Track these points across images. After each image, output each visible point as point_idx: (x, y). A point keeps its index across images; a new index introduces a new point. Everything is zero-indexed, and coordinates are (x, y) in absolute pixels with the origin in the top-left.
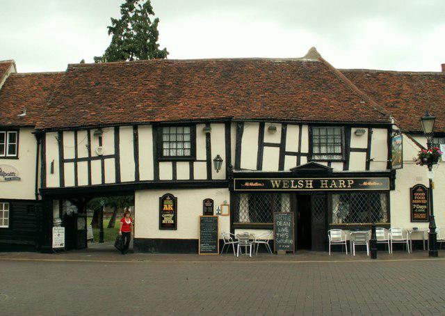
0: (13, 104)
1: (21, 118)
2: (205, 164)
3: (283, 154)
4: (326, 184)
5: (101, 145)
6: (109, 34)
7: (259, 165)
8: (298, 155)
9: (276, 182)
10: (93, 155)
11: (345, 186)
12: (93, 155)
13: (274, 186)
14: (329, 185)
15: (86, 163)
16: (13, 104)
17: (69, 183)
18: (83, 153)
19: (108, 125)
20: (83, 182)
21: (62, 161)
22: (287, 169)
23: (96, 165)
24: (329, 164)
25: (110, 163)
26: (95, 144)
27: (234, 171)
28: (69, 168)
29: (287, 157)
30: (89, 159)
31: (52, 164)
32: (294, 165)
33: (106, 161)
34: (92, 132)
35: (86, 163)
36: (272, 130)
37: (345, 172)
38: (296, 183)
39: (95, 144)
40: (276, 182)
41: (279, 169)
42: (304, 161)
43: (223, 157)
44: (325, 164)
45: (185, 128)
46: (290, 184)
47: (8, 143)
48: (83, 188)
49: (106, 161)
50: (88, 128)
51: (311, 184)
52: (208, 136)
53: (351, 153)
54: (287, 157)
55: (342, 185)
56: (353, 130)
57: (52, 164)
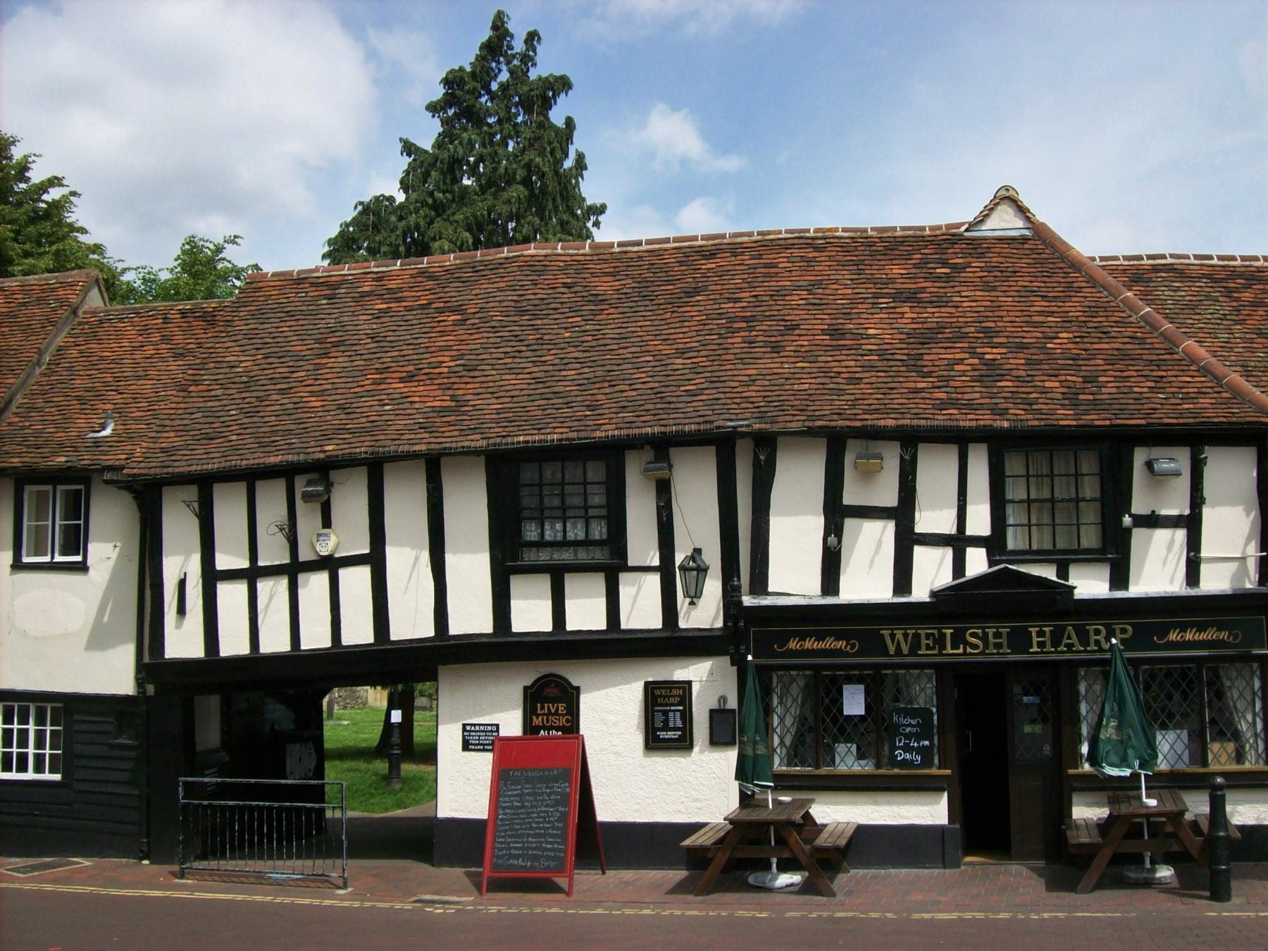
0: (78, 398)
1: (97, 443)
2: (654, 581)
3: (906, 541)
4: (1047, 639)
5: (327, 523)
6: (570, 123)
7: (1054, 546)
8: (958, 542)
9: (899, 634)
10: (305, 555)
11: (1049, 648)
12: (305, 555)
13: (892, 649)
14: (1056, 641)
15: (241, 588)
16: (78, 398)
17: (234, 644)
18: (273, 552)
19: (347, 463)
20: (275, 641)
21: (212, 577)
22: (920, 592)
23: (273, 592)
24: (1063, 573)
25: (356, 581)
26: (308, 522)
27: (747, 601)
28: (232, 596)
29: (919, 552)
30: (293, 570)
31: (182, 584)
32: (945, 578)
33: (345, 574)
34: (300, 486)
35: (241, 588)
36: (868, 475)
37: (1119, 594)
38: (958, 639)
39: (308, 522)
40: (899, 634)
41: (955, 577)
42: (977, 563)
43: (712, 557)
44: (1048, 572)
45: (590, 465)
46: (940, 641)
47: (58, 522)
48: (276, 659)
49: (345, 574)
50: (287, 473)
51: (1035, 639)
52: (664, 490)
53: (570, 627)
54: (919, 552)
55: (1097, 643)
56: (1140, 457)
57: (182, 584)
